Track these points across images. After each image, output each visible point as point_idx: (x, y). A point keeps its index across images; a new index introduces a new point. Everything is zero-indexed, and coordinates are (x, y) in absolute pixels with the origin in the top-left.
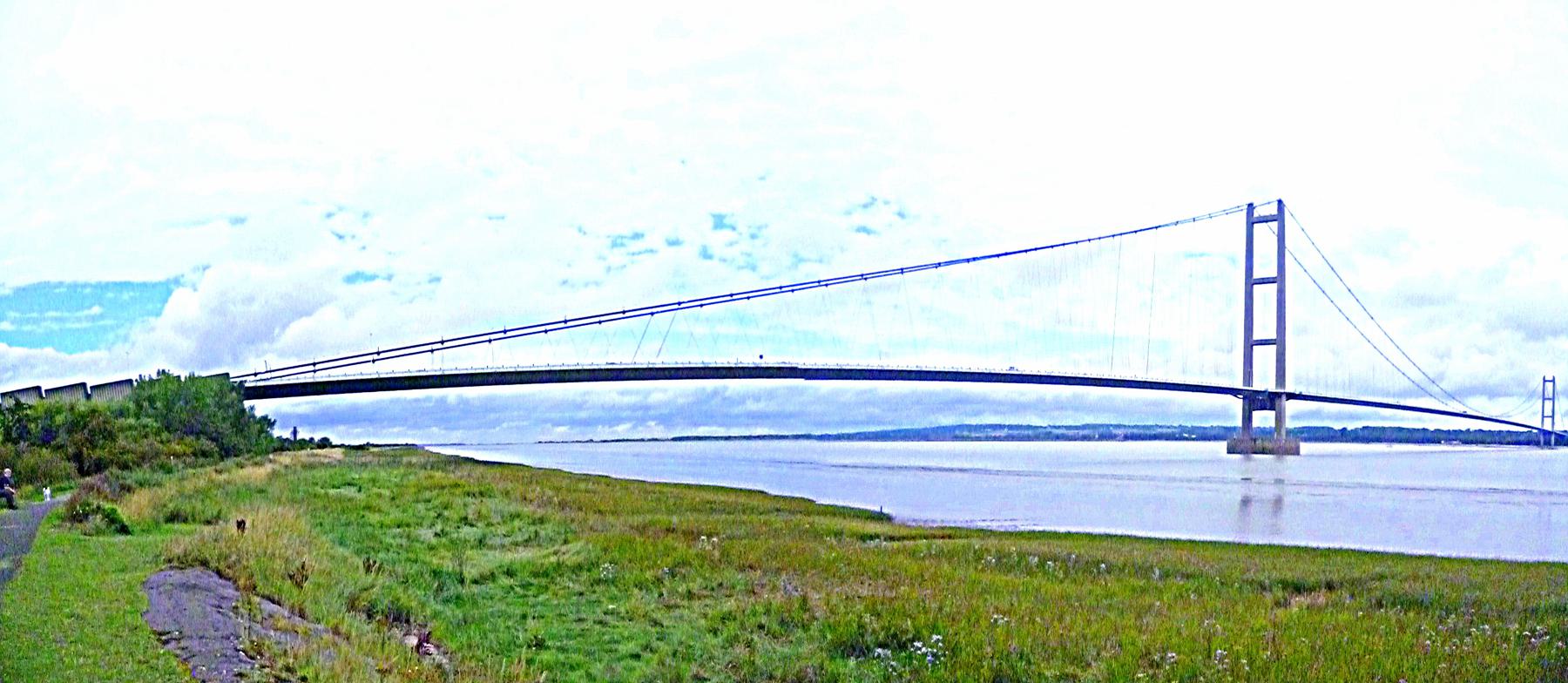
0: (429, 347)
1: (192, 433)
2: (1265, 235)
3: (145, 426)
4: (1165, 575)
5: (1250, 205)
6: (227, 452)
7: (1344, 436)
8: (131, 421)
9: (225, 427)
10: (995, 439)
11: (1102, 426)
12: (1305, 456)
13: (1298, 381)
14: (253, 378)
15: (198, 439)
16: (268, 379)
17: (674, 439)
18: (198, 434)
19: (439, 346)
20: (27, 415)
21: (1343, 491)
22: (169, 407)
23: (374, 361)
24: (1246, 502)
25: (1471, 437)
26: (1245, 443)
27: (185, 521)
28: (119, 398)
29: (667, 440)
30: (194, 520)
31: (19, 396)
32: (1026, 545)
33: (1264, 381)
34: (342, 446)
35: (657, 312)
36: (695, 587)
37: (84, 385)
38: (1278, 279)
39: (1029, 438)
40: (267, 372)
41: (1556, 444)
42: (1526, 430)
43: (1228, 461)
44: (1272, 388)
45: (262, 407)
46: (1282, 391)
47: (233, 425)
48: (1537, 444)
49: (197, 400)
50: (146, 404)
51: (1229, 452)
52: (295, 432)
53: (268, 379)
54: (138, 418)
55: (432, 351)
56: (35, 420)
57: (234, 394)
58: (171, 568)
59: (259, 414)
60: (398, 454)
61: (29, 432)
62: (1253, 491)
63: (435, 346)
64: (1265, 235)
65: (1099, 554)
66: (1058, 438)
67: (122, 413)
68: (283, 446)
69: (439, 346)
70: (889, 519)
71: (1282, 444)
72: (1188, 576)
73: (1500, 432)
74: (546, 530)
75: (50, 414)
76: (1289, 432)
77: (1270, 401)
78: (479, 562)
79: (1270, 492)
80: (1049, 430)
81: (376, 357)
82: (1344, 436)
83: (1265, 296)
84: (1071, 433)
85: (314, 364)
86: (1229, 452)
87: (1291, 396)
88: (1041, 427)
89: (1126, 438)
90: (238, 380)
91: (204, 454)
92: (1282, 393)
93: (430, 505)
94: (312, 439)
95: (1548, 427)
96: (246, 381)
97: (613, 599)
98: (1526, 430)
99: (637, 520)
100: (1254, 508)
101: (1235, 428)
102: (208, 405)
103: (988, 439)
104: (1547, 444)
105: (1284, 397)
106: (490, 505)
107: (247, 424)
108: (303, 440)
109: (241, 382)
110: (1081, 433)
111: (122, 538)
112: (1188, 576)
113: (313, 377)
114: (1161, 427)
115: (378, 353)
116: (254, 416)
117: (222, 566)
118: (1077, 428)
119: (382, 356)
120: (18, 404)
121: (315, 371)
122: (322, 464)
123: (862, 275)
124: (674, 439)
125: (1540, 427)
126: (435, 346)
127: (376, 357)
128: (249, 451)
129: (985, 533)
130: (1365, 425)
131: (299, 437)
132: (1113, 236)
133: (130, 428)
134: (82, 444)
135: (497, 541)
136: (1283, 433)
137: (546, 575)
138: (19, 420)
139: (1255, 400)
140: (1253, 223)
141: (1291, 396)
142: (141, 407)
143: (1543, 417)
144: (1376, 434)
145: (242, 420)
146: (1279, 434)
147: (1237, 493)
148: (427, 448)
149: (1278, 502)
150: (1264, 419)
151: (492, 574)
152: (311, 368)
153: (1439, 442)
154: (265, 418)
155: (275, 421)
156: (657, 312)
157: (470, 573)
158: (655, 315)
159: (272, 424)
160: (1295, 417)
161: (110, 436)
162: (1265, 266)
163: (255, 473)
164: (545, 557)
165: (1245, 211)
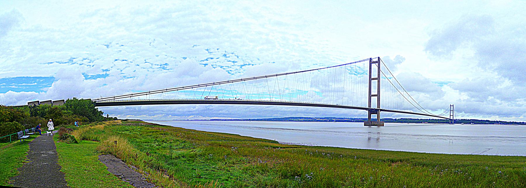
0: (146, 94)
1: (82, 115)
2: (374, 67)
3: (69, 113)
4: (357, 158)
5: (371, 58)
6: (91, 121)
7: (396, 121)
8: (66, 111)
9: (91, 114)
10: (301, 121)
11: (330, 118)
12: (385, 126)
13: (383, 107)
14: (97, 100)
15: (83, 117)
16: (101, 101)
17: (211, 120)
18: (83, 115)
19: (149, 93)
20: (37, 109)
21: (397, 136)
22: (75, 108)
23: (131, 97)
24: (369, 139)
25: (430, 121)
26: (369, 123)
27: (87, 140)
28: (62, 105)
29: (209, 120)
30: (90, 140)
31: (35, 103)
32: (320, 150)
33: (374, 106)
34: (120, 120)
35: (208, 86)
36: (234, 160)
37: (51, 101)
38: (378, 79)
39: (310, 121)
40: (101, 99)
41: (454, 123)
42: (446, 119)
43: (364, 128)
44: (376, 108)
45: (100, 109)
46: (379, 109)
47: (93, 113)
48: (449, 123)
49: (84, 106)
50: (69, 107)
51: (365, 125)
52: (108, 116)
53: (101, 101)
54: (67, 111)
55: (147, 94)
56: (39, 110)
57: (93, 105)
58: (103, 155)
59: (99, 110)
60: (138, 123)
61: (37, 113)
62: (372, 136)
63: (147, 93)
64: (374, 67)
65: (340, 153)
66: (318, 121)
67: (63, 109)
68: (106, 119)
69: (149, 93)
70: (277, 142)
71: (379, 123)
72: (364, 158)
73: (438, 119)
74: (187, 145)
75: (44, 108)
76: (381, 120)
77: (376, 111)
78: (176, 153)
79: (376, 136)
80: (315, 119)
81: (131, 96)
82: (396, 121)
83: (374, 83)
84: (321, 120)
85: (114, 97)
86: (365, 125)
87: (381, 110)
88: (313, 118)
89: (336, 121)
90: (94, 101)
91: (85, 121)
92: (379, 109)
93: (151, 137)
94: (112, 118)
95: (452, 118)
96: (96, 101)
97: (213, 164)
98: (446, 119)
99: (210, 142)
100: (372, 140)
101: (366, 119)
102: (86, 108)
103: (299, 121)
104: (452, 123)
105: (380, 110)
106: (168, 137)
107: (96, 113)
108: (110, 118)
109: (95, 101)
110: (324, 120)
111: (76, 144)
112: (364, 158)
113: (114, 101)
114: (346, 118)
115: (132, 95)
116: (98, 111)
117: (116, 154)
118: (323, 118)
119: (133, 95)
120: (35, 105)
121: (114, 99)
122: (117, 124)
123: (266, 76)
124: (211, 120)
125: (449, 118)
126: (147, 93)
127: (131, 96)
128: (97, 120)
129: (306, 147)
130: (402, 118)
131: (109, 117)
132: (334, 67)
133: (65, 113)
134: (53, 117)
135: (175, 148)
136: (379, 120)
137: (193, 157)
138: (35, 110)
139: (372, 111)
140: (371, 63)
141: (381, 110)
142: (68, 107)
143: (450, 115)
144: (405, 120)
145: (95, 112)
146: (378, 121)
147: (367, 136)
148: (143, 121)
149: (378, 139)
150: (374, 116)
151: (179, 157)
152: (113, 98)
153: (422, 123)
154: (101, 111)
155: (103, 112)
156: (208, 86)
157: (173, 156)
158: (221, 84)
159: (102, 113)
160: (375, 116)
161: (61, 115)
162: (375, 75)
163: (100, 127)
164: (190, 152)
165: (369, 60)
